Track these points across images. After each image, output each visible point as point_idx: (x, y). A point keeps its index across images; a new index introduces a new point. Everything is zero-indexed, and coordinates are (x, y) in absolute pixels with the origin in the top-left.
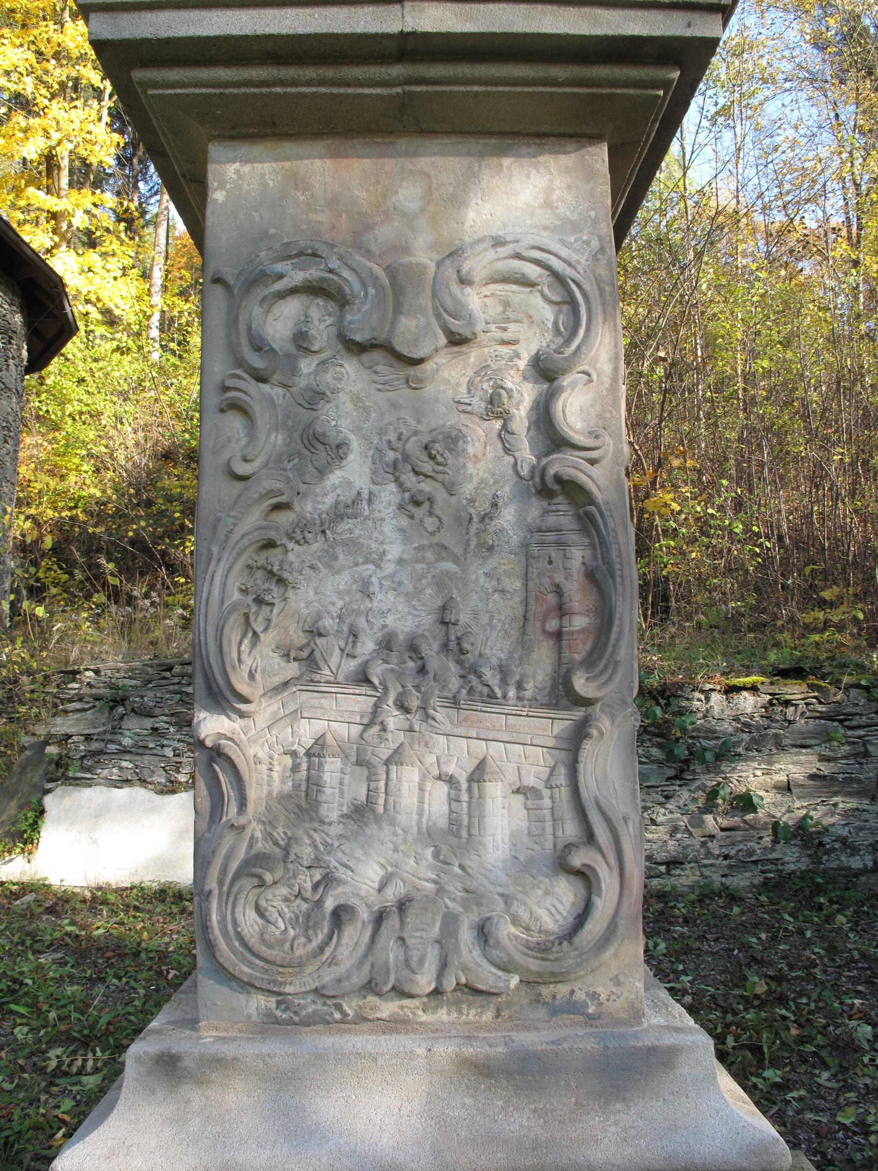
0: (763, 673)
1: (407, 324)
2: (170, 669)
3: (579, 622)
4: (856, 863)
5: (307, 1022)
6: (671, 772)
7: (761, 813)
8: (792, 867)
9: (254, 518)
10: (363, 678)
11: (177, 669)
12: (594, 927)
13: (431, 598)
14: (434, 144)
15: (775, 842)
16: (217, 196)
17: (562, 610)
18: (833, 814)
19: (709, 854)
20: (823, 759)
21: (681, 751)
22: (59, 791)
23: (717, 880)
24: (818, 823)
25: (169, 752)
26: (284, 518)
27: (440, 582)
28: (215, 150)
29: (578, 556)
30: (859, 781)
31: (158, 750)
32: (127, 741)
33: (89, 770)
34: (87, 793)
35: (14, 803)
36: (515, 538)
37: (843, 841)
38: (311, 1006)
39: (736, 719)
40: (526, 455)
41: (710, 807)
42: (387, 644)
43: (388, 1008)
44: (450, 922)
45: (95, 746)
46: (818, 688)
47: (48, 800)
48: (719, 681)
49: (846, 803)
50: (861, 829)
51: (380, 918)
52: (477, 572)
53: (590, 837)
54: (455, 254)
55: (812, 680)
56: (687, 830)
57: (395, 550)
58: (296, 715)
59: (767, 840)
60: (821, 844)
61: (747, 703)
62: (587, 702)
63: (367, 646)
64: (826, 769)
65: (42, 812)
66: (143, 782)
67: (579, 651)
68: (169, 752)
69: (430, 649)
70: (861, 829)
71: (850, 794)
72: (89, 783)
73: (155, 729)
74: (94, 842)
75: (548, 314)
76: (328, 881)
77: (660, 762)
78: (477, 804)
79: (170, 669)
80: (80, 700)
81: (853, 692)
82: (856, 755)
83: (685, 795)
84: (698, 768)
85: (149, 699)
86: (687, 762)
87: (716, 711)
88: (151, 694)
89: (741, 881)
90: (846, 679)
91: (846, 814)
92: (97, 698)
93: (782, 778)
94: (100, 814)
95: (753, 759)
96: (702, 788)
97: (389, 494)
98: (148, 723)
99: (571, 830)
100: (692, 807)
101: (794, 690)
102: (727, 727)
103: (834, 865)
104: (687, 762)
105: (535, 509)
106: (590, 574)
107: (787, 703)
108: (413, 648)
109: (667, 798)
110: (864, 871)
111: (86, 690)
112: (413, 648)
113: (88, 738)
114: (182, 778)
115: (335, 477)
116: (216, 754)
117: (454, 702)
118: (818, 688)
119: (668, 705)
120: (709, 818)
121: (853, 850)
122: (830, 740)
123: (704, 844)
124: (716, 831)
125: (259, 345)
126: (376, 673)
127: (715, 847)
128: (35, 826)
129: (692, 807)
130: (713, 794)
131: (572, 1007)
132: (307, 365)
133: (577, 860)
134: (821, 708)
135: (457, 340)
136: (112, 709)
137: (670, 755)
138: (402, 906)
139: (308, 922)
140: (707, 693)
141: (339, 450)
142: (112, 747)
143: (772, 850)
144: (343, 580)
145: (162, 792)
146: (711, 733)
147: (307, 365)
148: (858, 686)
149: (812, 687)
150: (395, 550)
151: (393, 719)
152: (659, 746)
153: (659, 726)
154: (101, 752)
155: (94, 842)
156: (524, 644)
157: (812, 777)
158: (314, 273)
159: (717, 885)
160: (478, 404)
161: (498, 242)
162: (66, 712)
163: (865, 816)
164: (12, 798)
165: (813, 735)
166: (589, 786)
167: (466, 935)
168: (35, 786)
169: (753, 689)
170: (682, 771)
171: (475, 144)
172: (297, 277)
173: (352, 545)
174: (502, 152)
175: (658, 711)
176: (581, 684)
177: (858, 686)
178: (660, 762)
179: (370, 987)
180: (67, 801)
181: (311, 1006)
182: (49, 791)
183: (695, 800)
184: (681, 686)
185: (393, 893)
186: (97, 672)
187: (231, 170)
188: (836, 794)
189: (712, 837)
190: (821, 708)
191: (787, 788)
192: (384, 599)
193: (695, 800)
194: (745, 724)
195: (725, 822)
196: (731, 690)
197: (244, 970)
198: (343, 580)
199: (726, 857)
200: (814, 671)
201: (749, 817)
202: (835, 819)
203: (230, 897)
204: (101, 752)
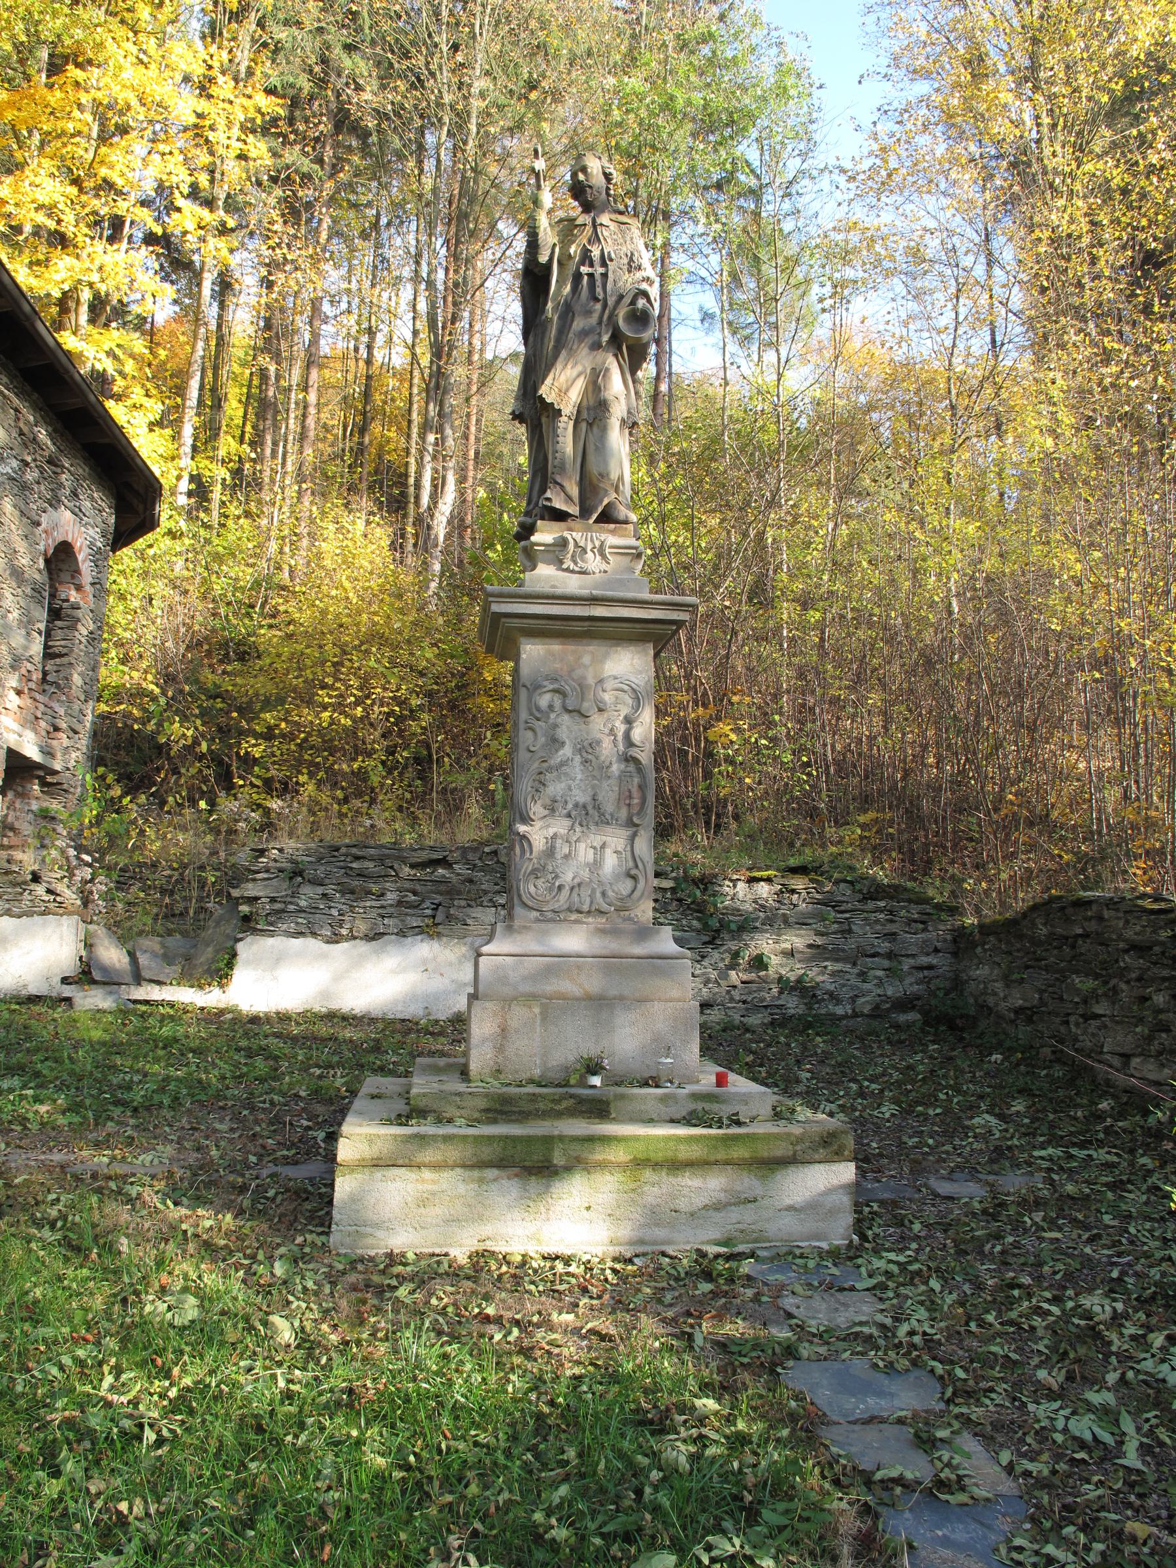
0: (778, 870)
1: (586, 705)
2: (337, 850)
3: (636, 801)
4: (839, 1011)
5: (549, 921)
6: (707, 939)
7: (771, 971)
8: (792, 1011)
9: (536, 765)
10: (569, 816)
11: (343, 850)
12: (637, 894)
13: (590, 792)
14: (596, 642)
15: (781, 993)
16: (524, 656)
17: (630, 797)
18: (823, 973)
19: (732, 1000)
20: (819, 934)
21: (714, 923)
22: (249, 939)
23: (737, 1018)
24: (812, 980)
25: (335, 912)
26: (545, 765)
27: (593, 787)
28: (522, 640)
29: (636, 780)
30: (843, 950)
31: (326, 911)
32: (303, 903)
33: (271, 924)
34: (270, 941)
35: (210, 949)
36: (617, 773)
37: (830, 994)
38: (550, 915)
39: (755, 901)
40: (621, 747)
41: (733, 966)
42: (576, 805)
43: (574, 917)
44: (594, 891)
45: (278, 906)
46: (817, 881)
47: (240, 947)
48: (743, 875)
49: (831, 966)
50: (844, 985)
51: (572, 889)
52: (605, 784)
53: (637, 867)
54: (601, 681)
55: (813, 876)
56: (716, 982)
57: (579, 777)
58: (548, 826)
59: (775, 991)
60: (814, 996)
61: (763, 890)
62: (637, 825)
63: (570, 806)
64: (819, 941)
65: (234, 955)
66: (314, 934)
67: (635, 810)
68: (335, 912)
69: (590, 808)
70: (844, 985)
71: (837, 960)
72: (272, 934)
73: (324, 895)
74: (276, 978)
75: (630, 701)
76: (557, 877)
77: (698, 931)
78: (602, 858)
79: (337, 850)
80: (267, 871)
81: (842, 885)
82: (842, 932)
83: (716, 955)
84: (726, 936)
85: (321, 872)
86: (718, 931)
87: (741, 895)
88: (322, 868)
89: (754, 1020)
90: (836, 875)
91: (833, 974)
92: (281, 870)
93: (787, 946)
94: (279, 959)
95: (766, 931)
96: (729, 951)
97: (578, 759)
98: (320, 890)
99: (631, 864)
100: (721, 965)
101: (799, 883)
102: (748, 907)
103: (823, 1011)
104: (718, 931)
105: (623, 766)
106: (640, 787)
107: (793, 891)
108: (584, 807)
109: (703, 957)
110: (846, 1017)
111: (272, 864)
112: (584, 807)
113: (273, 900)
114: (344, 932)
115: (561, 753)
116: (524, 837)
117: (597, 824)
118: (817, 881)
119: (706, 889)
120: (733, 973)
121: (838, 1001)
122: (824, 920)
123: (728, 992)
124: (738, 983)
125: (538, 709)
126: (573, 813)
127: (736, 994)
128: (230, 965)
129: (721, 965)
130: (736, 955)
131: (630, 919)
132: (553, 716)
133: (633, 872)
134: (818, 896)
135: (600, 710)
136: (291, 878)
137: (706, 926)
138: (579, 885)
139: (550, 889)
140: (735, 882)
141: (563, 743)
142: (292, 907)
143: (779, 998)
144: (563, 785)
145: (328, 942)
146: (737, 911)
147: (553, 716)
148: (845, 881)
149: (812, 880)
150: (579, 777)
151: (578, 829)
152: (699, 919)
153: (698, 904)
154: (283, 911)
155: (276, 978)
156: (619, 808)
157: (810, 946)
158: (556, 686)
159: (737, 1022)
160: (607, 731)
161: (616, 678)
162: (254, 880)
163: (847, 976)
164: (208, 945)
165: (812, 915)
166: (637, 852)
167: (598, 895)
168: (228, 936)
169: (768, 880)
170: (714, 938)
171: (609, 642)
172: (551, 687)
173: (566, 774)
174: (617, 645)
175: (698, 893)
176: (635, 820)
177: (845, 881)
178: (698, 931)
179: (570, 910)
180: (255, 948)
181: (550, 915)
182: (241, 939)
183: (723, 959)
184: (715, 876)
185: (577, 881)
186: (281, 850)
187: (528, 647)
188: (827, 959)
189: (735, 987)
190: (818, 896)
191: (790, 954)
192: (575, 792)
193: (723, 959)
194: (762, 906)
195: (745, 977)
196: (752, 880)
197: (530, 903)
198: (563, 785)
199: (744, 1002)
200: (816, 870)
201: (763, 973)
202: (825, 977)
203: (527, 881)
204: (283, 911)
